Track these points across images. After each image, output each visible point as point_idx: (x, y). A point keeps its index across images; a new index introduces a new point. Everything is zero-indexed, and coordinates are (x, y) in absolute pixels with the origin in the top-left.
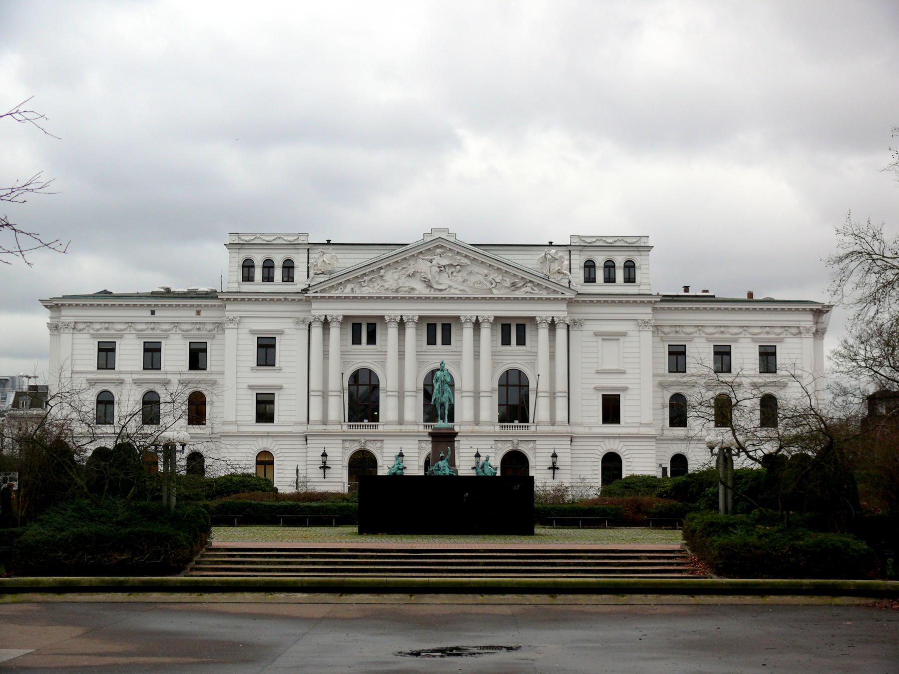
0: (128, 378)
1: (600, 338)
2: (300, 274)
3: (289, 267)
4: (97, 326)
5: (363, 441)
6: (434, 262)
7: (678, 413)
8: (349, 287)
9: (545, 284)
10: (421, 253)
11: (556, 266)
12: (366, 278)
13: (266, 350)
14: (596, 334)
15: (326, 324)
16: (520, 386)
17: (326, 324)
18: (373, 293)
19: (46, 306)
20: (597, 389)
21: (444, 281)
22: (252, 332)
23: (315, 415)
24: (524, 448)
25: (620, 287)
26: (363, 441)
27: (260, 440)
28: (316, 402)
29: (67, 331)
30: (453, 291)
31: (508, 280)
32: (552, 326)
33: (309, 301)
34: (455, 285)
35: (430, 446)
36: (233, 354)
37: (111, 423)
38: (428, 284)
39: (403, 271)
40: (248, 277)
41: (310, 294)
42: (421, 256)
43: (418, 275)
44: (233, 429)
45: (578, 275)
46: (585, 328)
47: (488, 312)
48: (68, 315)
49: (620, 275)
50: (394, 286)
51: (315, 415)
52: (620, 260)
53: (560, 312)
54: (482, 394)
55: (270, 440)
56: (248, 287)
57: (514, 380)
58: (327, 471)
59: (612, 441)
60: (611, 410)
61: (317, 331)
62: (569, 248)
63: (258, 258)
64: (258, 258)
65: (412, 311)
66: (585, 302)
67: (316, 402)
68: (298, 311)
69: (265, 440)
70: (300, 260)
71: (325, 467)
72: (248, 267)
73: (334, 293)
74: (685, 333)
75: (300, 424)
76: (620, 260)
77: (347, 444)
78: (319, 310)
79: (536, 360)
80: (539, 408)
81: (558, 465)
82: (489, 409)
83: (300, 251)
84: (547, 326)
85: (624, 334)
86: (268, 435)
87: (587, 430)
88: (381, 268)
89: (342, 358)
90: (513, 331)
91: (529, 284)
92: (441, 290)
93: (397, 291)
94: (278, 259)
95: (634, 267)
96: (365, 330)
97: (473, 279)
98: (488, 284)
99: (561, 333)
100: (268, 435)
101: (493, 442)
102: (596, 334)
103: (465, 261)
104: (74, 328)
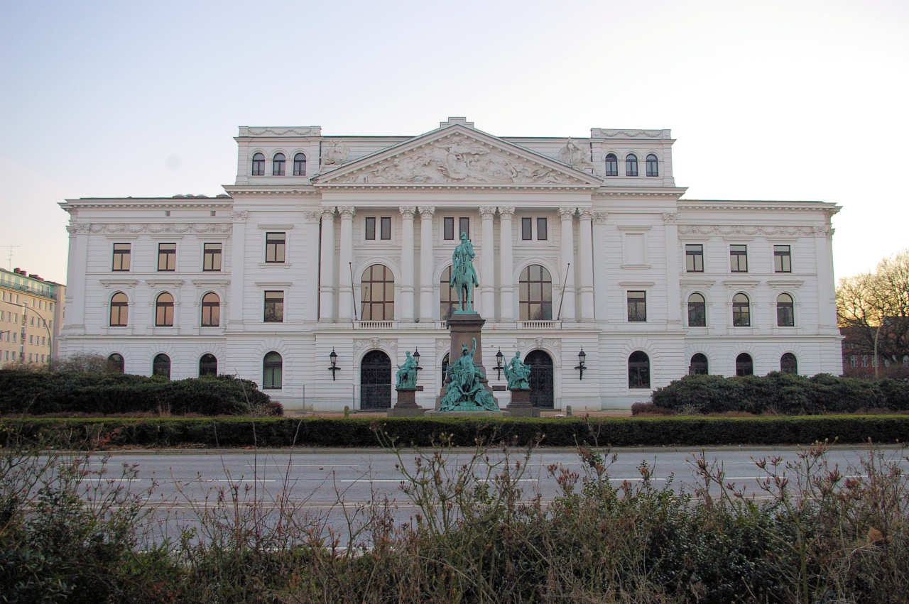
0: (142, 279)
1: (623, 233)
2: (311, 168)
3: (300, 160)
4: (113, 228)
5: (375, 340)
6: (452, 150)
7: (697, 314)
8: (361, 177)
9: (568, 172)
10: (437, 141)
11: (578, 156)
12: (380, 168)
13: (275, 241)
14: (620, 228)
15: (337, 216)
16: (541, 282)
17: (337, 216)
18: (387, 183)
19: (65, 209)
20: (622, 285)
21: (461, 170)
22: (261, 227)
23: (326, 313)
24: (548, 347)
25: (642, 181)
26: (375, 340)
27: (266, 339)
28: (326, 299)
29: (82, 232)
30: (472, 180)
31: (529, 169)
32: (576, 217)
33: (318, 193)
34: (472, 174)
35: (449, 345)
36: (244, 251)
37: (648, 386)
38: (444, 171)
39: (419, 161)
40: (258, 172)
41: (320, 184)
42: (437, 144)
43: (434, 164)
44: (239, 327)
45: (601, 167)
46: (607, 222)
47: (509, 202)
48: (85, 216)
49: (643, 168)
50: (408, 174)
51: (326, 313)
52: (642, 153)
53: (582, 201)
54: (502, 289)
55: (279, 339)
56: (257, 180)
57: (535, 276)
58: (336, 372)
59: (639, 339)
60: (637, 309)
61: (328, 223)
62: (590, 142)
63: (269, 151)
64: (269, 151)
65: (428, 201)
66: (608, 194)
67: (326, 299)
68: (308, 204)
69: (273, 339)
70: (311, 152)
71: (334, 369)
72: (258, 160)
73: (344, 183)
74: (702, 233)
75: (311, 322)
76: (642, 153)
77: (358, 344)
78: (330, 200)
79: (557, 252)
80: (564, 306)
81: (586, 364)
82: (510, 306)
83: (312, 143)
84: (571, 218)
85: (648, 228)
86: (275, 334)
87: (612, 328)
88: (395, 157)
89: (354, 251)
90: (534, 223)
91: (551, 174)
92: (458, 179)
93: (413, 179)
94: (290, 151)
95: (656, 161)
96: (378, 222)
97: (493, 168)
98: (509, 173)
99: (585, 224)
100: (275, 334)
101: (516, 341)
102: (620, 228)
103: (486, 149)
104: (90, 230)
